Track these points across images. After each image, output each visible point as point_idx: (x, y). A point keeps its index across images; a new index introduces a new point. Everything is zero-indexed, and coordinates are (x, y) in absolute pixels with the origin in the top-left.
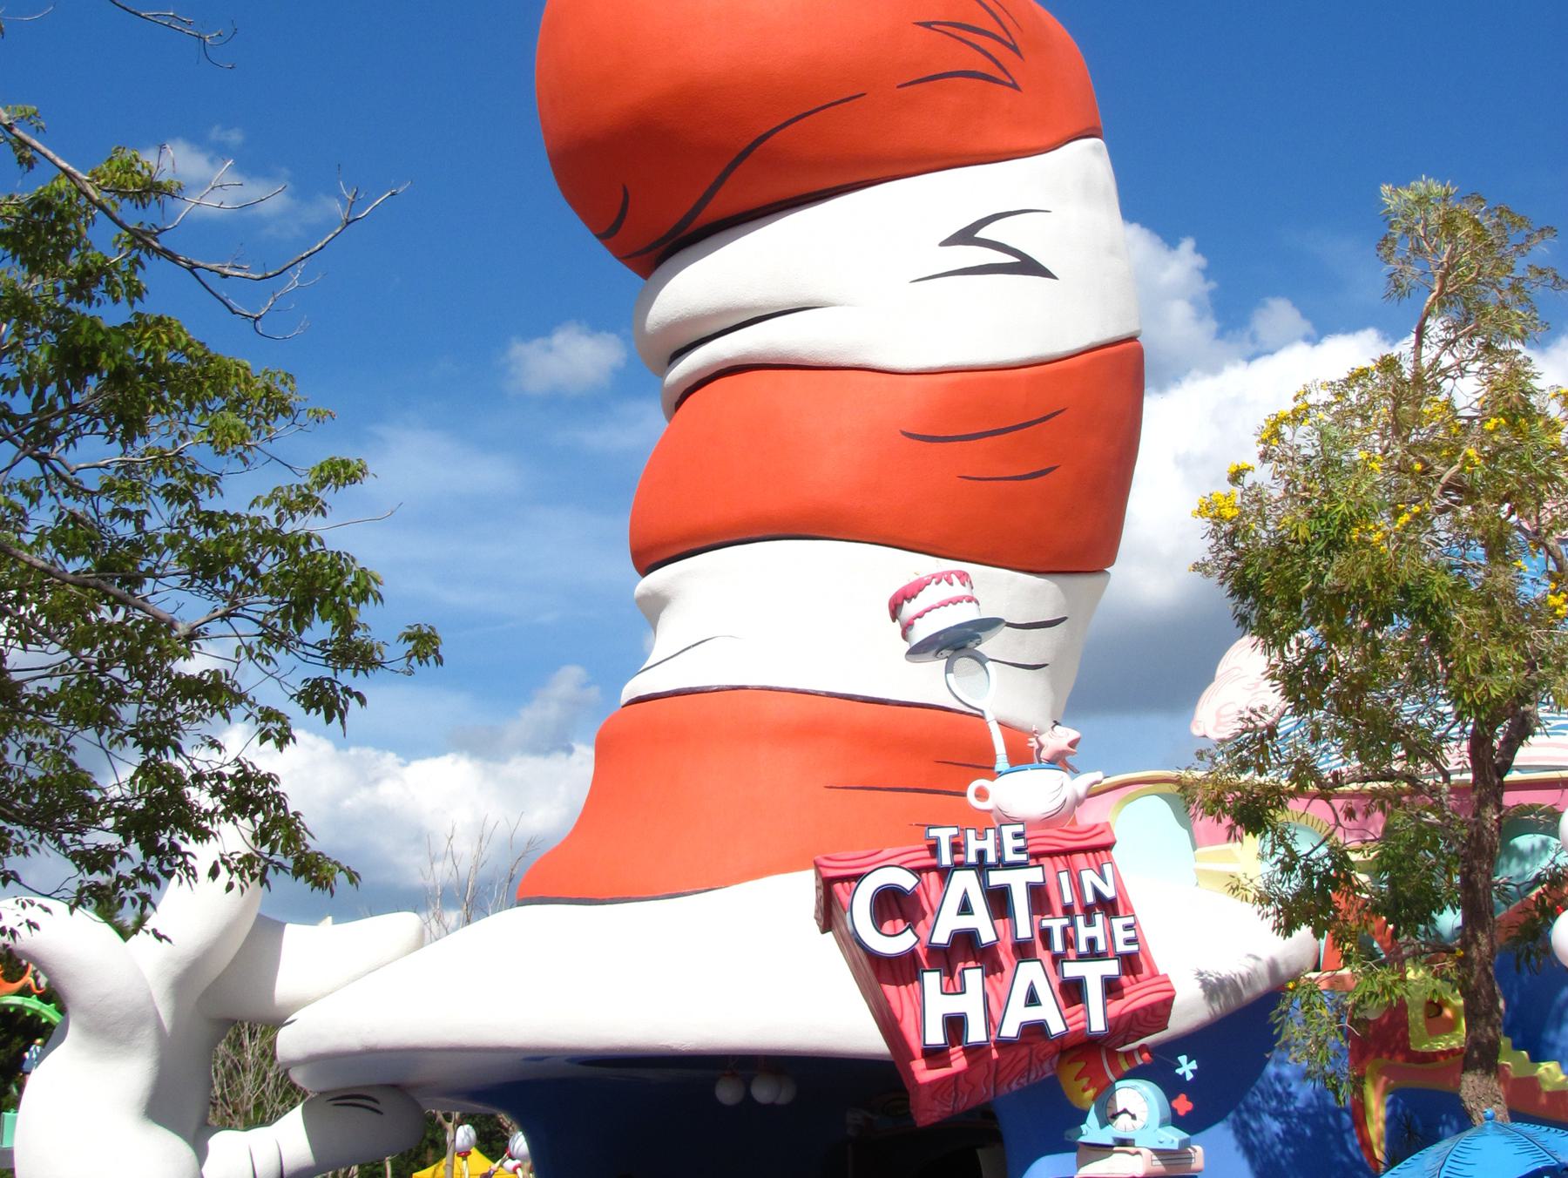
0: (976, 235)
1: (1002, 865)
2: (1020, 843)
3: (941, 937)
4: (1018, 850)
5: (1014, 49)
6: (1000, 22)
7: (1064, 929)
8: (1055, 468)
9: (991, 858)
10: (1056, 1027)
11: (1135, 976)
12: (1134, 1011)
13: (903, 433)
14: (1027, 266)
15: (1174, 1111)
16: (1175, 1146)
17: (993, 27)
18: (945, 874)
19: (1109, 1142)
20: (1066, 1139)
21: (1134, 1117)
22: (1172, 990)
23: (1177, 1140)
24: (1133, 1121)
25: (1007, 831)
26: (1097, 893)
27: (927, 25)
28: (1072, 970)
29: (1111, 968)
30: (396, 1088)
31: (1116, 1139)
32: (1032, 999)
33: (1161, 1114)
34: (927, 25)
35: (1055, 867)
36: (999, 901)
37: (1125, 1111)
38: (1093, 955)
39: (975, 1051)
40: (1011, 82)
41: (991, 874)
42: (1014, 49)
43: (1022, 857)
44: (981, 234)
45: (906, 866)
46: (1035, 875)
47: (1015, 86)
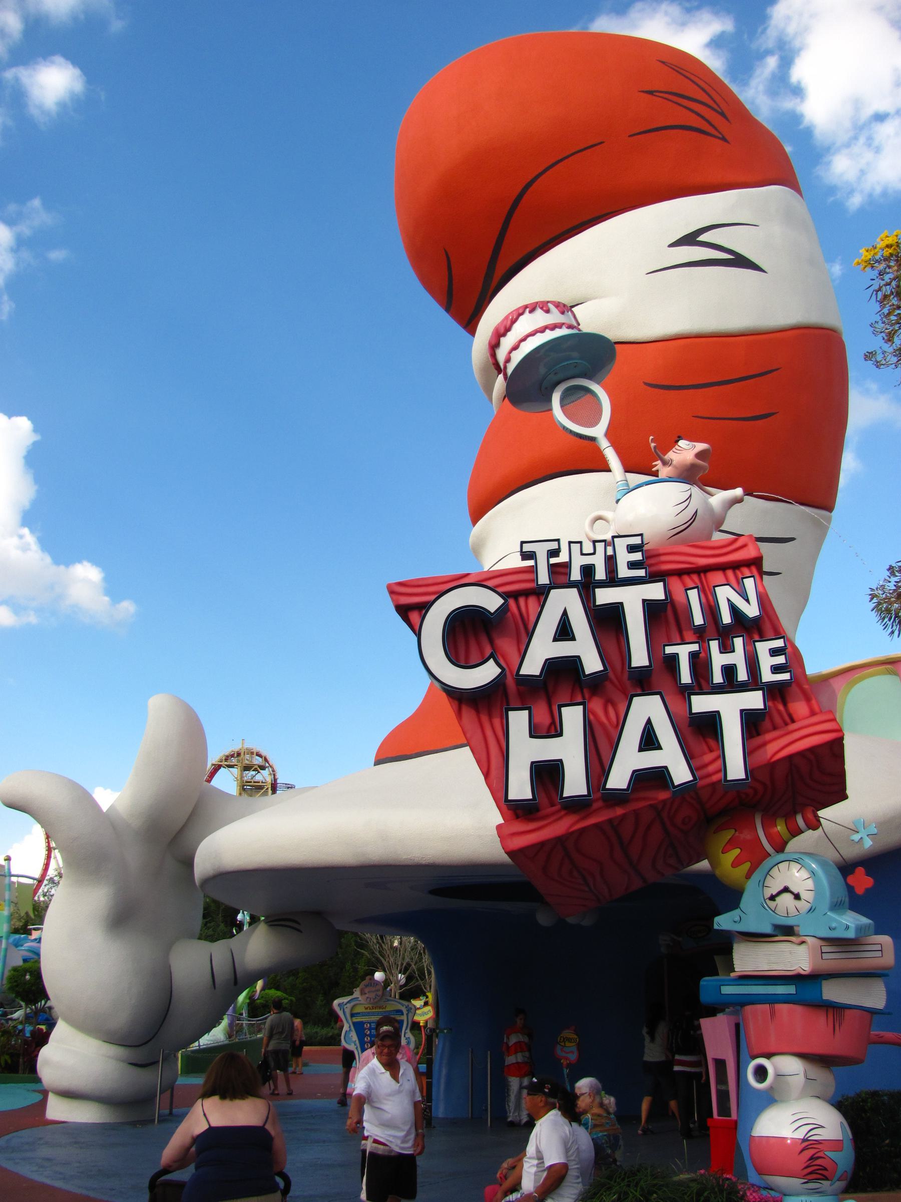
0: (698, 239)
1: (613, 581)
3: (532, 666)
4: (632, 565)
5: (722, 114)
6: (709, 96)
7: (693, 656)
8: (773, 414)
9: (600, 574)
10: (681, 774)
11: (785, 704)
12: (790, 757)
14: (739, 261)
15: (850, 889)
16: (851, 934)
17: (706, 99)
18: (541, 593)
19: (768, 930)
20: (716, 927)
21: (797, 897)
22: (840, 730)
23: (852, 926)
24: (797, 903)
26: (734, 610)
27: (650, 93)
28: (701, 704)
29: (754, 700)
31: (777, 927)
32: (649, 741)
33: (832, 894)
34: (650, 93)
35: (684, 584)
37: (786, 890)
38: (731, 684)
39: (576, 805)
40: (721, 136)
41: (598, 591)
42: (722, 114)
43: (641, 573)
44: (702, 238)
45: (500, 590)
46: (656, 591)
47: (724, 139)
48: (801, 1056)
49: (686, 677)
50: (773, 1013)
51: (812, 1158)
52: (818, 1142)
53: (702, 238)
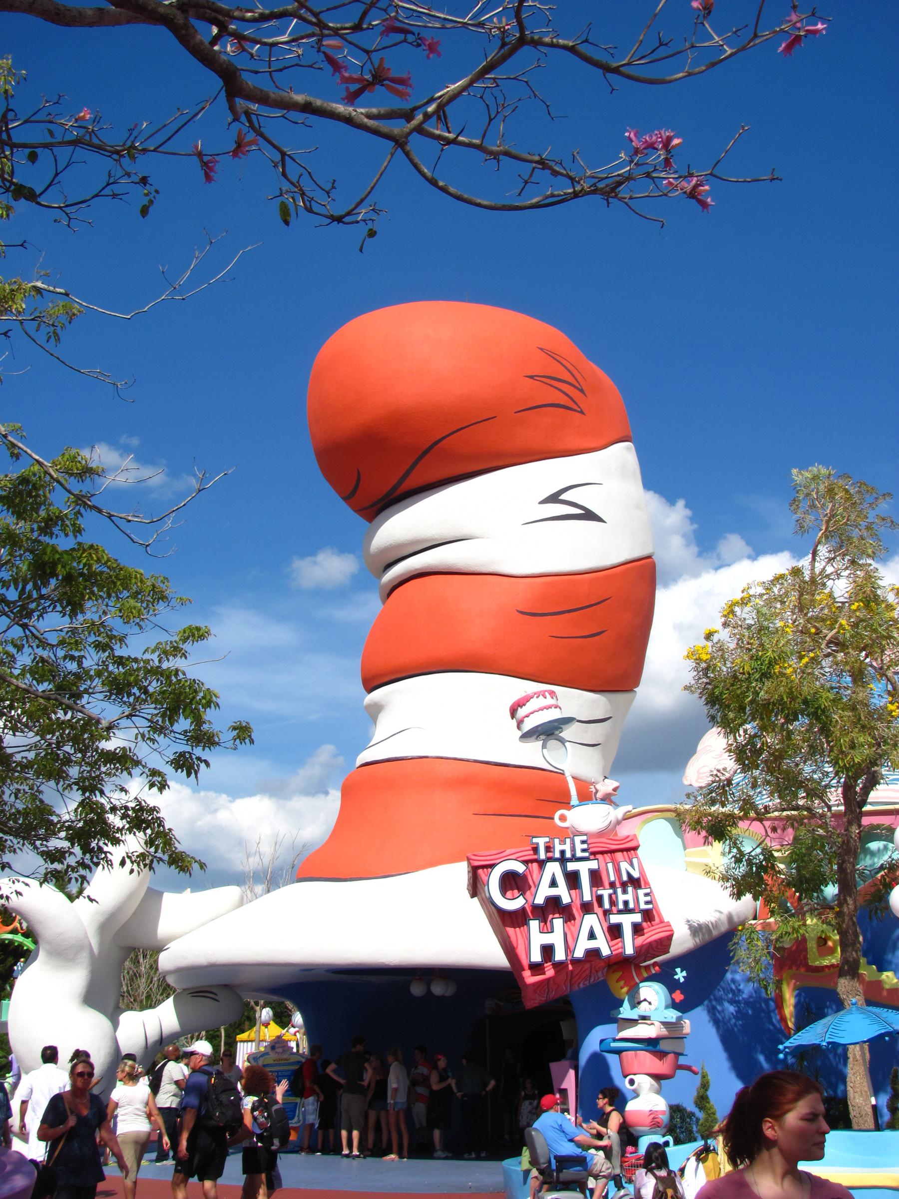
1: (574, 859)
2: (585, 846)
4: (584, 850)
5: (582, 391)
7: (610, 896)
9: (568, 855)
13: (518, 611)
14: (589, 515)
15: (673, 1000)
16: (674, 1020)
18: (542, 864)
19: (636, 1017)
21: (650, 1003)
22: (672, 931)
23: (675, 1017)
25: (578, 840)
26: (629, 874)
27: (531, 377)
28: (614, 919)
29: (637, 918)
30: (226, 986)
32: (592, 936)
34: (531, 377)
36: (573, 880)
37: (645, 1000)
38: (627, 910)
42: (582, 391)
43: (586, 854)
44: (563, 497)
46: (593, 865)
47: (582, 412)
48: (648, 1074)
49: (607, 905)
50: (636, 1055)
51: (654, 1118)
52: (656, 1111)
53: (563, 497)
